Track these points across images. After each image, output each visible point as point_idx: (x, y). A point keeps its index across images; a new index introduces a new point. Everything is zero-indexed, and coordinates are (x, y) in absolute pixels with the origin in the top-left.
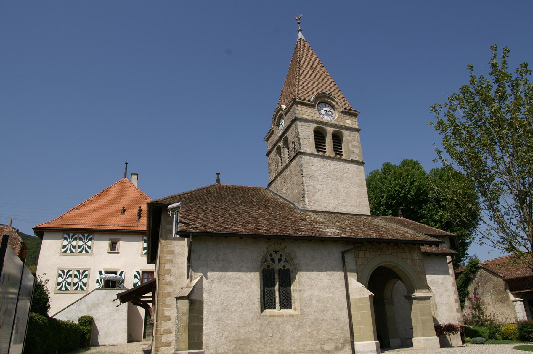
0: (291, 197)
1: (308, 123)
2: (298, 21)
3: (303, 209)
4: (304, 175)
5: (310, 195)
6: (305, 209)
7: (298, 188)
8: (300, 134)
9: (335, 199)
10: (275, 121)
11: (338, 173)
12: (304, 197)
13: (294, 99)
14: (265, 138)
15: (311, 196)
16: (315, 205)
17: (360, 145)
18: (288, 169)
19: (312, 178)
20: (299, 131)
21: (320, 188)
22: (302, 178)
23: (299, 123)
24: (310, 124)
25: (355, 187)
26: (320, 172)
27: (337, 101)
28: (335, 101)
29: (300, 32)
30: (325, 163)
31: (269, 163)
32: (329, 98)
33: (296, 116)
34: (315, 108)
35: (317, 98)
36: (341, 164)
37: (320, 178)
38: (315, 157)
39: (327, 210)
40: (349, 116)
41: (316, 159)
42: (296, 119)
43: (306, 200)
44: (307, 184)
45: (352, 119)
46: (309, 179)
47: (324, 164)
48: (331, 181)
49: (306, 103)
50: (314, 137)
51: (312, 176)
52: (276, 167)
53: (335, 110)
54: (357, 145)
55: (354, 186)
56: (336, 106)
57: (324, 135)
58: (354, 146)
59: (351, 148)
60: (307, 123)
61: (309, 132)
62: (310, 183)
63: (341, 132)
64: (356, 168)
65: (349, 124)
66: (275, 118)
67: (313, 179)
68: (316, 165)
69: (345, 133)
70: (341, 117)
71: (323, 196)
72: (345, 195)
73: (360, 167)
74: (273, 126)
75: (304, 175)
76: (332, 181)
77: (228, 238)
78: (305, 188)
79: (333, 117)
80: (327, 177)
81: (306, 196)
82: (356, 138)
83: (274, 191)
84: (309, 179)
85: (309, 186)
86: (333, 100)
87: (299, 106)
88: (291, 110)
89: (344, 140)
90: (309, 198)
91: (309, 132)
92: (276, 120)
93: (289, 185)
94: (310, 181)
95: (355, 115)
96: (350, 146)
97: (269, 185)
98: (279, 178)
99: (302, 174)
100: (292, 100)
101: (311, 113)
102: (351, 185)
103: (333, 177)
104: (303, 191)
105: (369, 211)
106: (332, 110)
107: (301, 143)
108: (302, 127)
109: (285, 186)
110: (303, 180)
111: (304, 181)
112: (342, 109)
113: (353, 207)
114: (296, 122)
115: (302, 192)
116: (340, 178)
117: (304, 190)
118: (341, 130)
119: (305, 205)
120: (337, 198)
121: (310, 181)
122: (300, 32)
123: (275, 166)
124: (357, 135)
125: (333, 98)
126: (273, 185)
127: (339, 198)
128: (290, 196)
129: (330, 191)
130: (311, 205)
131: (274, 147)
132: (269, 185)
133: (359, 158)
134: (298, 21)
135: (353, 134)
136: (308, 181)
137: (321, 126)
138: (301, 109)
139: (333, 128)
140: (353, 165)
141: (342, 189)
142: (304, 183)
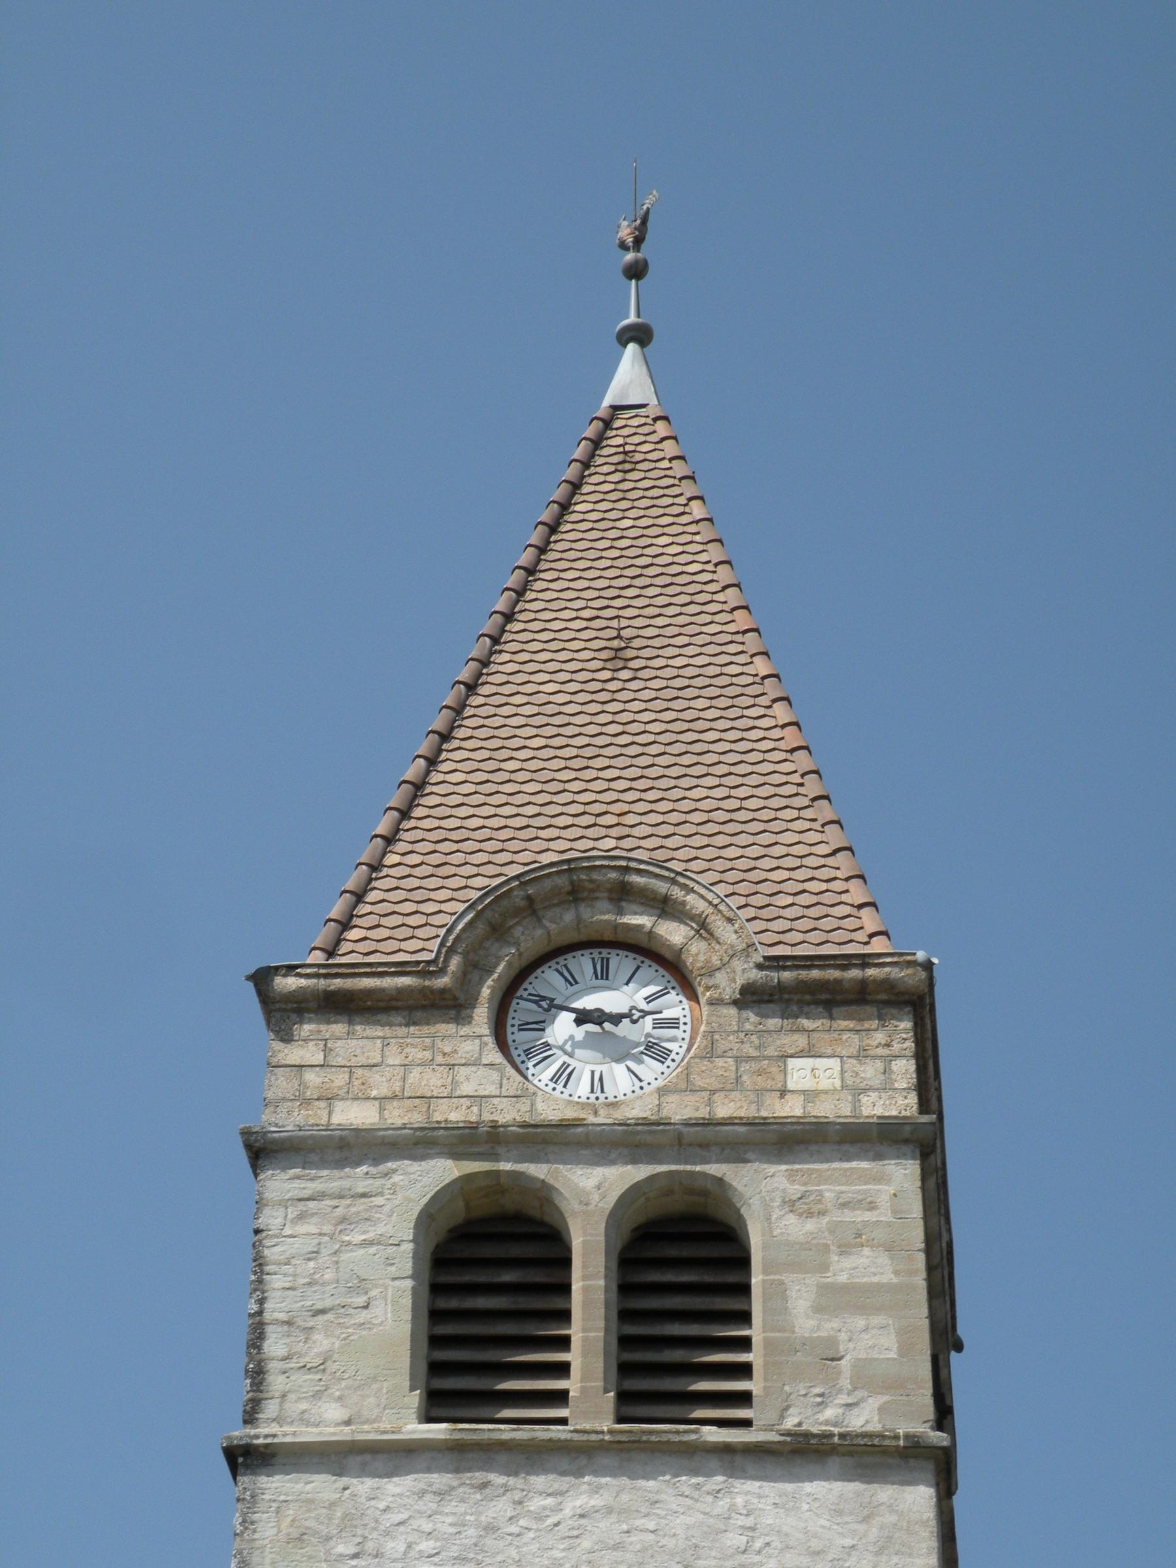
1: (376, 1162)
30: (500, 1508)
32: (623, 894)
125: (662, 887)
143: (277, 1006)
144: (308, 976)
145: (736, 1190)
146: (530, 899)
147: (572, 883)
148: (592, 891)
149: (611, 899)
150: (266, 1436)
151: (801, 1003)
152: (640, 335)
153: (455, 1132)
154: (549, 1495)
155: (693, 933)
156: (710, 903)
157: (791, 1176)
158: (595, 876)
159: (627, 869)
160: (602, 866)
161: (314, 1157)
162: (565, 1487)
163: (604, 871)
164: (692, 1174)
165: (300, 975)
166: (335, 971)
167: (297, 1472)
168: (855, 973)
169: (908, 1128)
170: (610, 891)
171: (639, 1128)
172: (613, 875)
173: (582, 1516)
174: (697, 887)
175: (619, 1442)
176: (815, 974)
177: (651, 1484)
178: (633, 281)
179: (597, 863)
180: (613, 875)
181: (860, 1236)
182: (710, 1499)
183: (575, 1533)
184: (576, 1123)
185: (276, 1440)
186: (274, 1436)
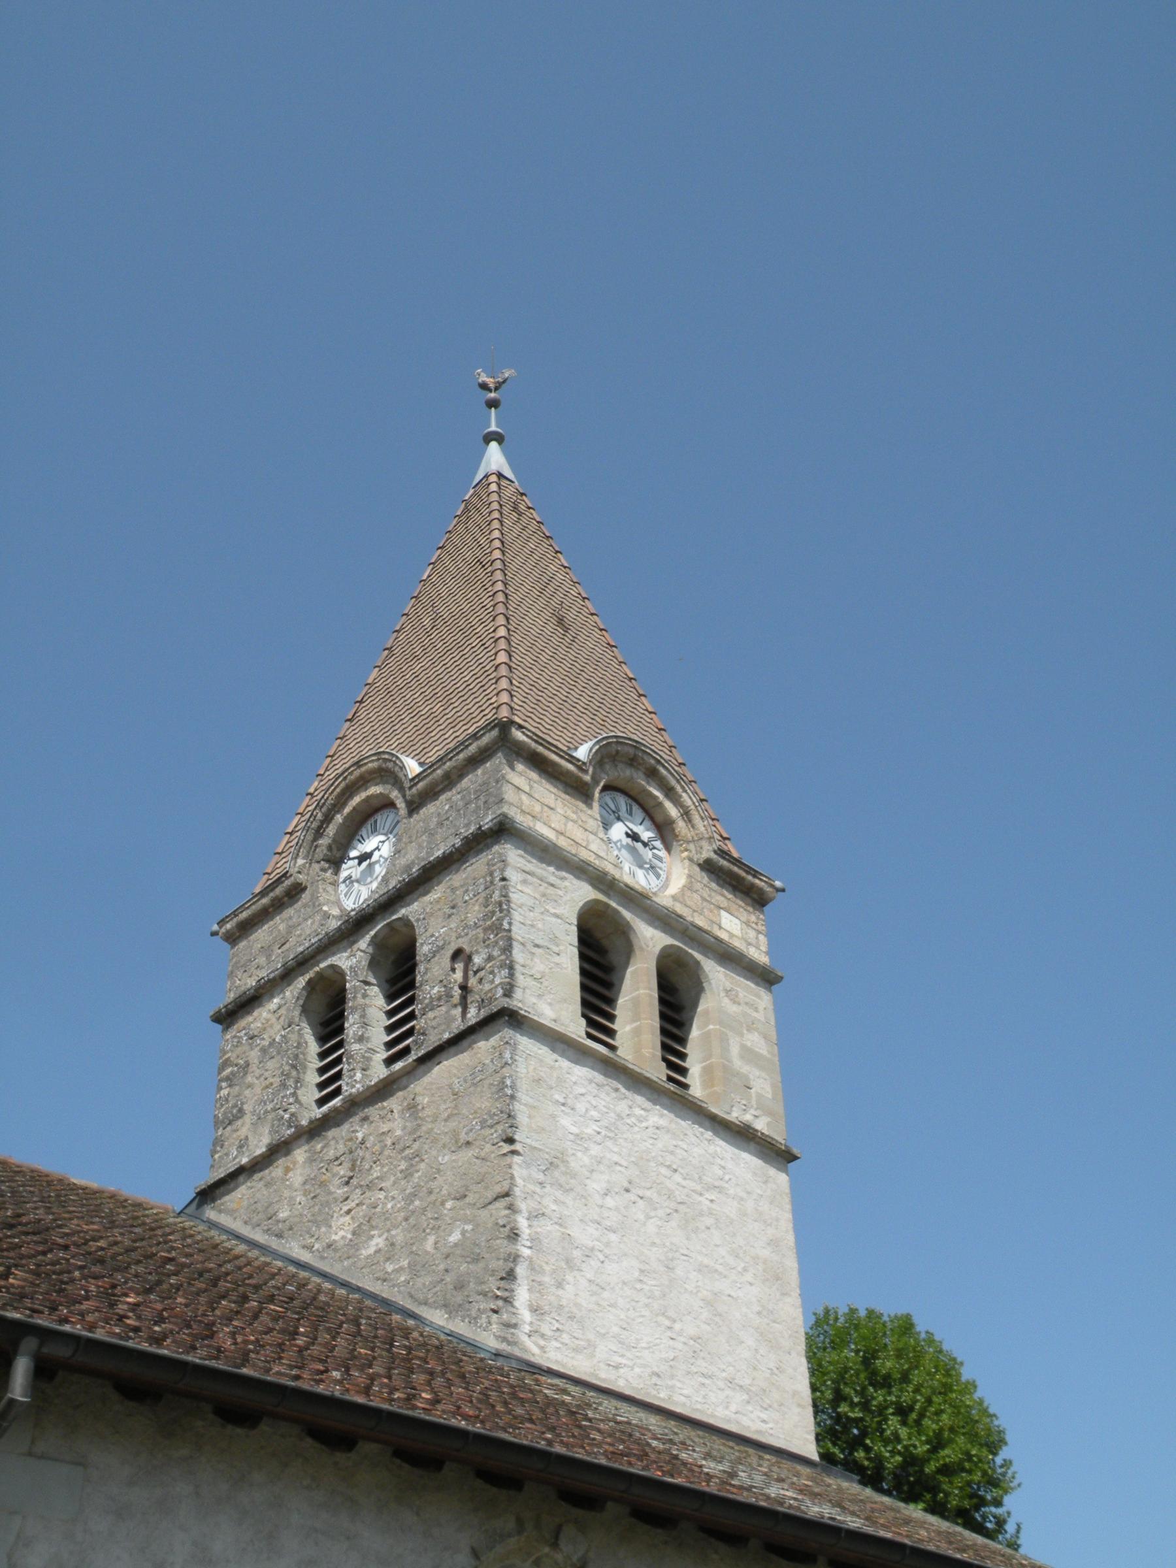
0: (400, 1270)
1: (559, 868)
2: (492, 395)
3: (503, 1347)
4: (517, 1147)
5: (542, 1272)
6: (517, 1352)
7: (466, 1221)
8: (516, 916)
9: (659, 1324)
10: (319, 833)
11: (677, 1178)
12: (510, 1276)
13: (504, 727)
14: (221, 923)
15: (547, 1279)
16: (565, 1337)
17: (776, 1059)
18: (394, 1103)
19: (556, 1174)
20: (514, 896)
21: (590, 1244)
22: (508, 1159)
23: (513, 855)
24: (562, 879)
25: (749, 1277)
26: (595, 1150)
27: (688, 802)
28: (677, 801)
29: (494, 445)
30: (622, 1106)
31: (226, 1063)
32: (652, 774)
33: (505, 816)
34: (590, 806)
35: (602, 758)
36: (689, 1132)
37: (596, 1185)
38: (576, 1062)
39: (621, 1386)
40: (730, 896)
41: (581, 1073)
42: (503, 830)
43: (522, 1295)
44: (532, 1204)
45: (744, 916)
46: (541, 1177)
47: (618, 1109)
48: (642, 1217)
49: (554, 764)
50: (576, 951)
51: (554, 1163)
52: (284, 1086)
53: (668, 848)
54: (765, 1053)
55: (745, 1270)
56: (681, 826)
57: (615, 958)
58: (748, 1054)
59: (738, 1064)
60: (552, 869)
61: (557, 916)
62: (545, 1201)
63: (698, 963)
64: (755, 1174)
65: (731, 935)
66: (328, 818)
67: (562, 1180)
68: (581, 1107)
69: (715, 974)
70: (698, 886)
71: (606, 1294)
72: (705, 1315)
73: (772, 1171)
74: (300, 862)
75: (517, 1147)
76: (648, 1217)
77: (264, 1427)
78: (522, 1222)
79: (658, 876)
80: (627, 1191)
81: (521, 1270)
82: (760, 1016)
83: (246, 1231)
84: (541, 1177)
85: (542, 1221)
86: (669, 792)
87: (520, 767)
88: (465, 783)
89: (707, 1012)
90: (537, 1286)
91: (557, 916)
92: (331, 830)
93: (389, 1200)
94: (548, 1189)
95: (757, 899)
96: (735, 1050)
97: (208, 1195)
98: (300, 1154)
99: (510, 1141)
100: (488, 727)
101: (570, 824)
102: (731, 1261)
103: (655, 1197)
104: (509, 1237)
105: (812, 1437)
106: (658, 844)
107: (517, 967)
108: (524, 882)
109: (351, 1204)
110: (512, 1177)
111: (519, 1181)
112: (707, 852)
113: (741, 1397)
114: (496, 848)
115: (503, 1245)
116: (681, 1208)
117: (514, 1236)
118: (697, 955)
119: (515, 1326)
120: (667, 1323)
121: (548, 1189)
122: (494, 445)
123: (276, 1081)
124: (763, 999)
125: (673, 782)
126: (241, 1195)
127: (677, 1326)
128: (390, 1268)
129: (637, 1274)
130: (543, 1336)
131: (287, 975)
132: (208, 1195)
133: (768, 1124)
134: (492, 395)
135: (747, 989)
136: (538, 1189)
137: (614, 904)
138: (527, 789)
139: (664, 932)
140: (746, 1156)
141: (693, 1275)
142: (517, 1191)
143: (508, 745)
144: (527, 736)
145: (704, 971)
146: (617, 752)
147: (635, 755)
148: (640, 764)
149: (645, 774)
150: (526, 1011)
151: (724, 880)
152: (499, 438)
153: (596, 871)
154: (643, 1109)
155: (679, 815)
156: (694, 803)
157: (726, 975)
158: (645, 757)
159: (658, 762)
160: (649, 754)
161: (529, 848)
162: (649, 1108)
163: (649, 757)
164: (687, 952)
165: (523, 733)
166: (541, 741)
167: (535, 1040)
168: (750, 878)
169: (773, 976)
170: (647, 769)
171: (673, 915)
172: (652, 762)
173: (657, 1128)
174: (688, 791)
175: (676, 1094)
176: (736, 869)
177: (683, 1123)
178: (493, 409)
179: (648, 751)
180: (652, 762)
181: (753, 1024)
182: (706, 1142)
183: (655, 1137)
184: (646, 897)
185: (530, 1016)
186: (529, 1013)
